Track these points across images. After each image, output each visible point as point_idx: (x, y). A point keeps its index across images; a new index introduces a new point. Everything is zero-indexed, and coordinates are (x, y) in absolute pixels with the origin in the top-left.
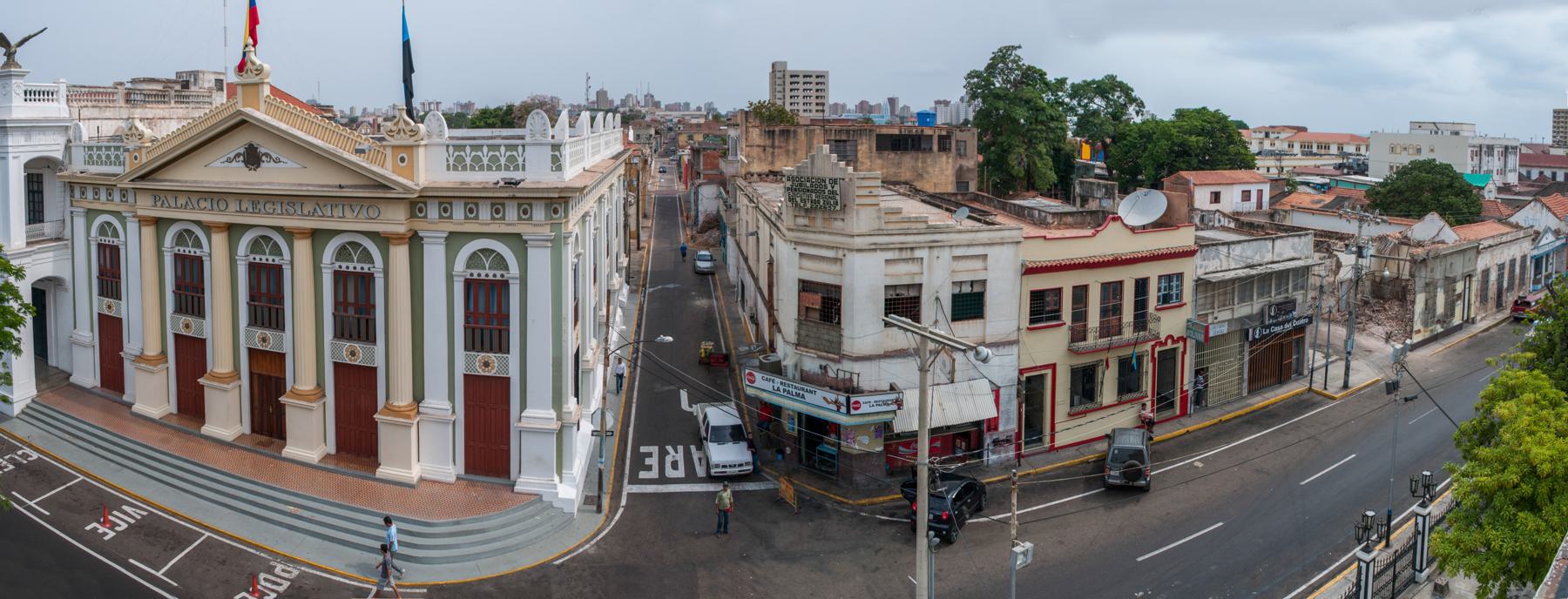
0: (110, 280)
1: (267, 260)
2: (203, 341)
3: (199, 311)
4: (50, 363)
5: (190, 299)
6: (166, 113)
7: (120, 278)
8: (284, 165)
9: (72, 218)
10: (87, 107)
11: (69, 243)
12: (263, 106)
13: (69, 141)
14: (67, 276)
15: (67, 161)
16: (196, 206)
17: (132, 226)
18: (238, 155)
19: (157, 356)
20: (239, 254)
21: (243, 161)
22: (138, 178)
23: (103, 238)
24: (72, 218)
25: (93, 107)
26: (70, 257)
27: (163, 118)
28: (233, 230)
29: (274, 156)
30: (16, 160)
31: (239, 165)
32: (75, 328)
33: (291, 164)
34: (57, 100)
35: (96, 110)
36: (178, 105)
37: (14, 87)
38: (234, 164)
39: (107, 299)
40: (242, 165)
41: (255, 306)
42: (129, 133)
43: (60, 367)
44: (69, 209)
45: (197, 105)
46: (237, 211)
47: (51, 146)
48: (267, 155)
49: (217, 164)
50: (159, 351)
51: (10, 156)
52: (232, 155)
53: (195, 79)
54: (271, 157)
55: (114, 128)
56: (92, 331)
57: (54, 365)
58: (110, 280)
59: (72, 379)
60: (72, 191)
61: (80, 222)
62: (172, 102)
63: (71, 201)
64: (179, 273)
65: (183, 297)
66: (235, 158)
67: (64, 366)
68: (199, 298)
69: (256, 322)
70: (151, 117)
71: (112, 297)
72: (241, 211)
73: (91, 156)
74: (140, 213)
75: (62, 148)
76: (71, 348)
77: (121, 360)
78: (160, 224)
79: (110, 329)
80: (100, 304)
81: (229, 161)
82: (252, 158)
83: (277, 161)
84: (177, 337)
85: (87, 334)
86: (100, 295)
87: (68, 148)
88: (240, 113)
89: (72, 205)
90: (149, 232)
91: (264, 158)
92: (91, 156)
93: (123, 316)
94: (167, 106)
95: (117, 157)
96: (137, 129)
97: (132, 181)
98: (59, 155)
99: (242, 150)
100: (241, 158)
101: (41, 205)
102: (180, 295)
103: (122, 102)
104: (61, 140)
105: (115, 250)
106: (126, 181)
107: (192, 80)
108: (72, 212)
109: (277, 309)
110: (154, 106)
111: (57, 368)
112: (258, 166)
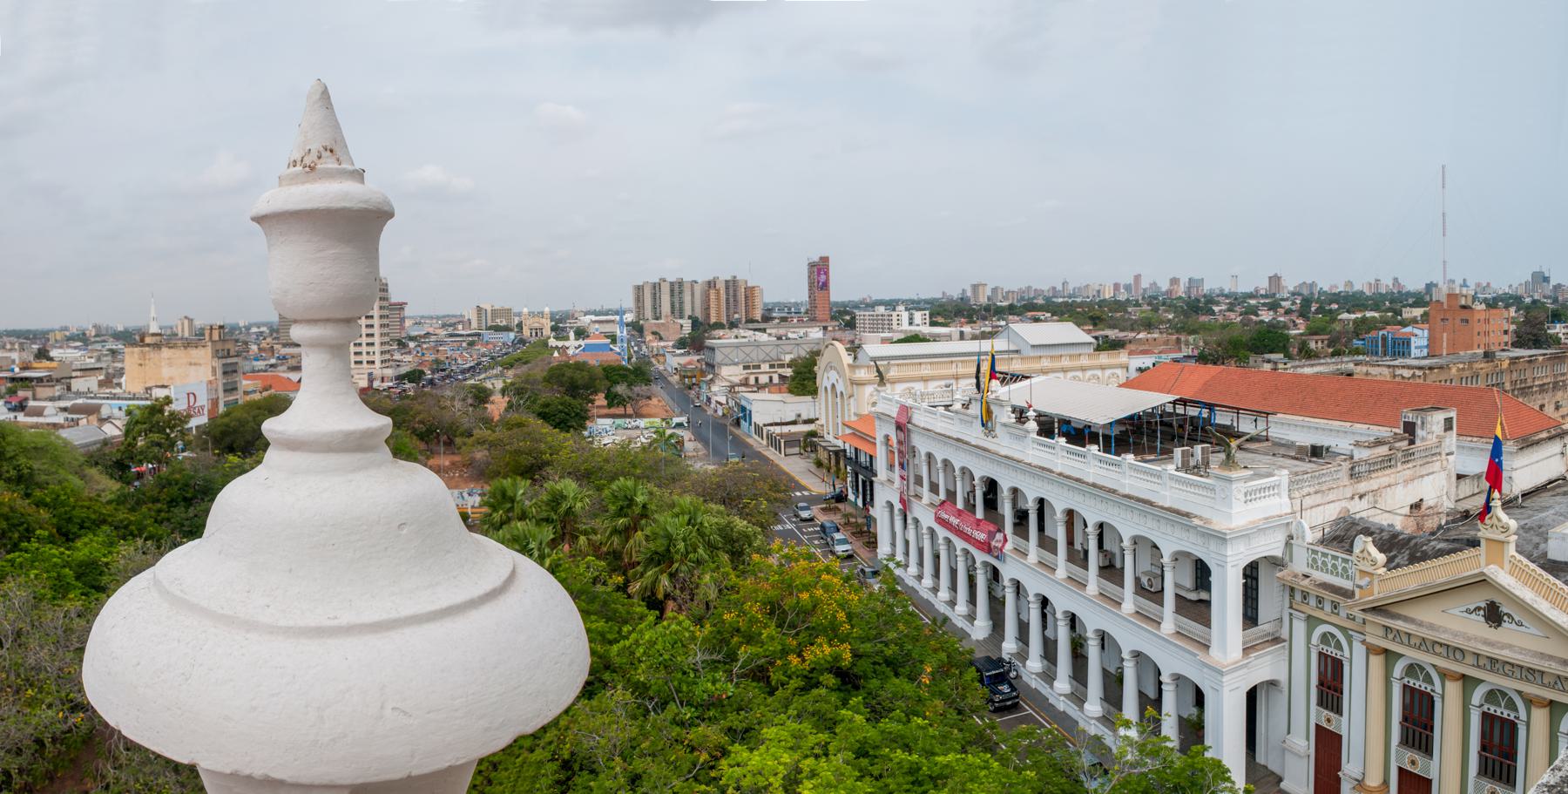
0: (1330, 689)
1: (1502, 713)
2: (1429, 782)
3: (1427, 749)
4: (1257, 760)
5: (1417, 734)
6: (1391, 480)
7: (1342, 693)
8: (1527, 630)
9: (1291, 620)
10: (1309, 494)
11: (1286, 644)
12: (1507, 566)
13: (1291, 537)
14: (1282, 677)
15: (1287, 558)
16: (1431, 649)
17: (1359, 651)
18: (1479, 608)
19: (1379, 787)
20: (1473, 703)
21: (1484, 616)
22: (1374, 608)
23: (1325, 648)
24: (1291, 620)
25: (1316, 493)
26: (1287, 658)
27: (1389, 486)
28: (1468, 683)
29: (1517, 619)
30: (1234, 569)
31: (1479, 618)
32: (1289, 733)
33: (1533, 630)
34: (1278, 494)
35: (1319, 495)
36: (1405, 466)
37: (1235, 492)
38: (1473, 616)
39: (1326, 712)
40: (1483, 619)
41: (1486, 758)
42: (1360, 555)
43: (1269, 767)
44: (1287, 611)
45: (1425, 460)
46: (1473, 665)
47: (1271, 546)
48: (1509, 616)
49: (1456, 611)
50: (1381, 781)
51: (1229, 565)
52: (1472, 608)
53: (1423, 423)
54: (1513, 619)
55: (1338, 510)
56: (1308, 739)
57: (1263, 762)
58: (1330, 689)
59: (1283, 785)
60: (1292, 597)
61: (1300, 627)
62: (1399, 464)
63: (1291, 603)
64: (1408, 701)
65: (1411, 731)
66: (1475, 610)
67: (1273, 767)
68: (1427, 736)
69: (1486, 773)
70: (1376, 488)
71: (1332, 710)
72: (1478, 666)
73: (1314, 560)
74: (1369, 639)
75: (1282, 545)
76: (1284, 754)
77: (1338, 780)
78: (1390, 656)
79: (1328, 746)
80: (1318, 715)
81: (1469, 611)
82: (1493, 615)
83: (1520, 624)
84: (1401, 771)
85: (1303, 744)
86: (1318, 705)
87: (1288, 545)
88: (1483, 574)
89: (1291, 607)
90: (1377, 662)
91: (1505, 618)
92: (1314, 560)
93: (1344, 733)
94: (1393, 470)
95: (1344, 569)
96: (1369, 554)
97: (1363, 610)
98: (1278, 553)
99: (1483, 605)
100: (1482, 612)
101: (1254, 592)
102: (1407, 728)
103: (1346, 481)
104: (1280, 537)
105: (1338, 665)
106: (1356, 609)
107: (1419, 422)
108: (1291, 614)
109: (1509, 765)
110: (1380, 474)
111: (1265, 767)
112: (1499, 625)
